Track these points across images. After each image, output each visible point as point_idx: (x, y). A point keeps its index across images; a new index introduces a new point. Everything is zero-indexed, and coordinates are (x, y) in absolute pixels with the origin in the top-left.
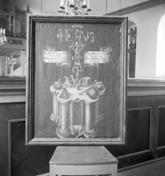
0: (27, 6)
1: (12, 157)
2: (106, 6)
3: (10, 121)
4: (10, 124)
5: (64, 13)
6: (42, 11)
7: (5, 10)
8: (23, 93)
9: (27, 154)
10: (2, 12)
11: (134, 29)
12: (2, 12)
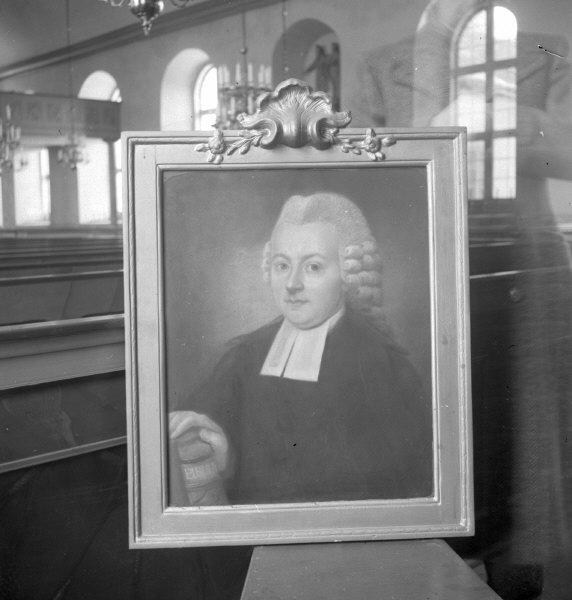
2: (243, 50)
8: (114, 337)
11: (329, 50)
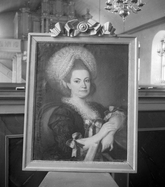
0: (87, 9)
1: (9, 180)
3: (7, 137)
4: (8, 141)
5: (112, 10)
6: (100, 13)
7: (50, 14)
8: (20, 102)
9: (29, 178)
10: (61, 17)
12: (61, 17)
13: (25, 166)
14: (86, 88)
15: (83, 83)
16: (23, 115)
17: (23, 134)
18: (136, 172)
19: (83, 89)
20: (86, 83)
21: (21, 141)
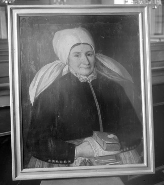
8: (4, 93)
13: (16, 176)
14: (89, 64)
15: (85, 57)
16: (9, 107)
17: (10, 130)
18: (154, 173)
19: (87, 66)
20: (89, 57)
21: (7, 139)
